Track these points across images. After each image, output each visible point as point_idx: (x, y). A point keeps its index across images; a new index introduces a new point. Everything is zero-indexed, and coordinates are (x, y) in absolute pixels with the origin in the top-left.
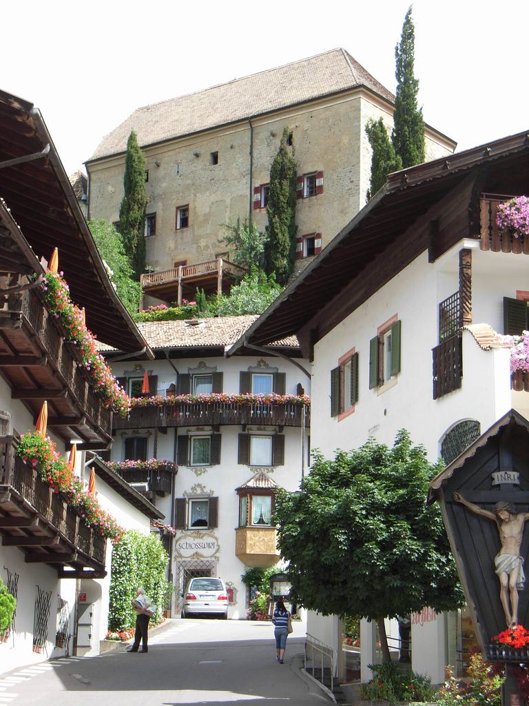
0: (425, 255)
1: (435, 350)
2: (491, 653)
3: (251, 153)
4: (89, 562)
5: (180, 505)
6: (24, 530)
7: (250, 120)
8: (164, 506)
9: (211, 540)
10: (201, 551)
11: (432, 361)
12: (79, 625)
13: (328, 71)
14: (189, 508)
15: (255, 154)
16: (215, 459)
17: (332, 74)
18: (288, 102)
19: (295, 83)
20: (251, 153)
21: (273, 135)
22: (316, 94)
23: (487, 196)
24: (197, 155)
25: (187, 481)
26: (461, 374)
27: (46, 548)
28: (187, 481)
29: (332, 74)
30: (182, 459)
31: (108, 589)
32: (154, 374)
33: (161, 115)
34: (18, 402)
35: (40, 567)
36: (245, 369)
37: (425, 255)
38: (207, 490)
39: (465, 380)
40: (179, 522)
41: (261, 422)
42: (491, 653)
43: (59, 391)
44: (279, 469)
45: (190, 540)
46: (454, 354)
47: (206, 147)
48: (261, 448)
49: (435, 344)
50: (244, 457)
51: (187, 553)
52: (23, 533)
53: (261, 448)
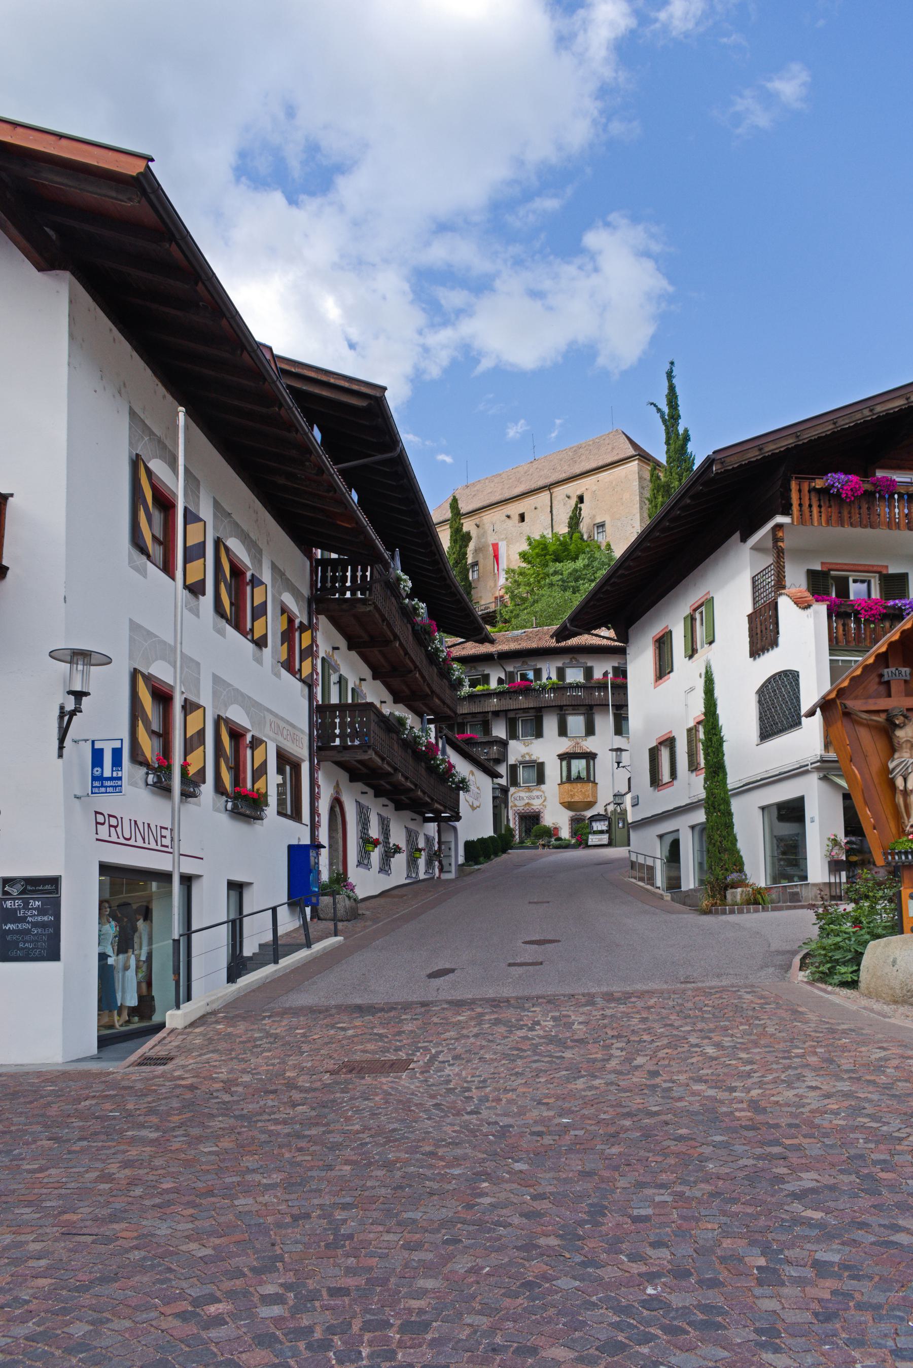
0: (737, 535)
1: (750, 617)
2: (890, 858)
3: (551, 511)
4: (446, 808)
5: (513, 769)
6: (388, 783)
7: (549, 487)
8: (502, 769)
9: (539, 793)
10: (532, 802)
11: (747, 626)
12: (607, 832)
13: (610, 447)
14: (520, 770)
15: (554, 512)
16: (539, 734)
17: (613, 448)
18: (578, 471)
19: (583, 457)
20: (551, 511)
21: (569, 497)
22: (601, 463)
23: (796, 478)
24: (508, 517)
25: (517, 750)
26: (778, 633)
27: (410, 798)
28: (517, 750)
29: (613, 448)
30: (513, 735)
31: (830, 528)
32: (486, 672)
33: (478, 490)
34: (378, 682)
35: (408, 814)
36: (560, 664)
37: (737, 535)
38: (534, 758)
39: (781, 639)
40: (514, 782)
41: (576, 708)
42: (890, 858)
43: (411, 671)
44: (591, 738)
45: (522, 794)
46: (770, 616)
47: (514, 509)
48: (576, 723)
49: (750, 610)
50: (563, 731)
51: (520, 804)
52: (388, 787)
53: (576, 723)
